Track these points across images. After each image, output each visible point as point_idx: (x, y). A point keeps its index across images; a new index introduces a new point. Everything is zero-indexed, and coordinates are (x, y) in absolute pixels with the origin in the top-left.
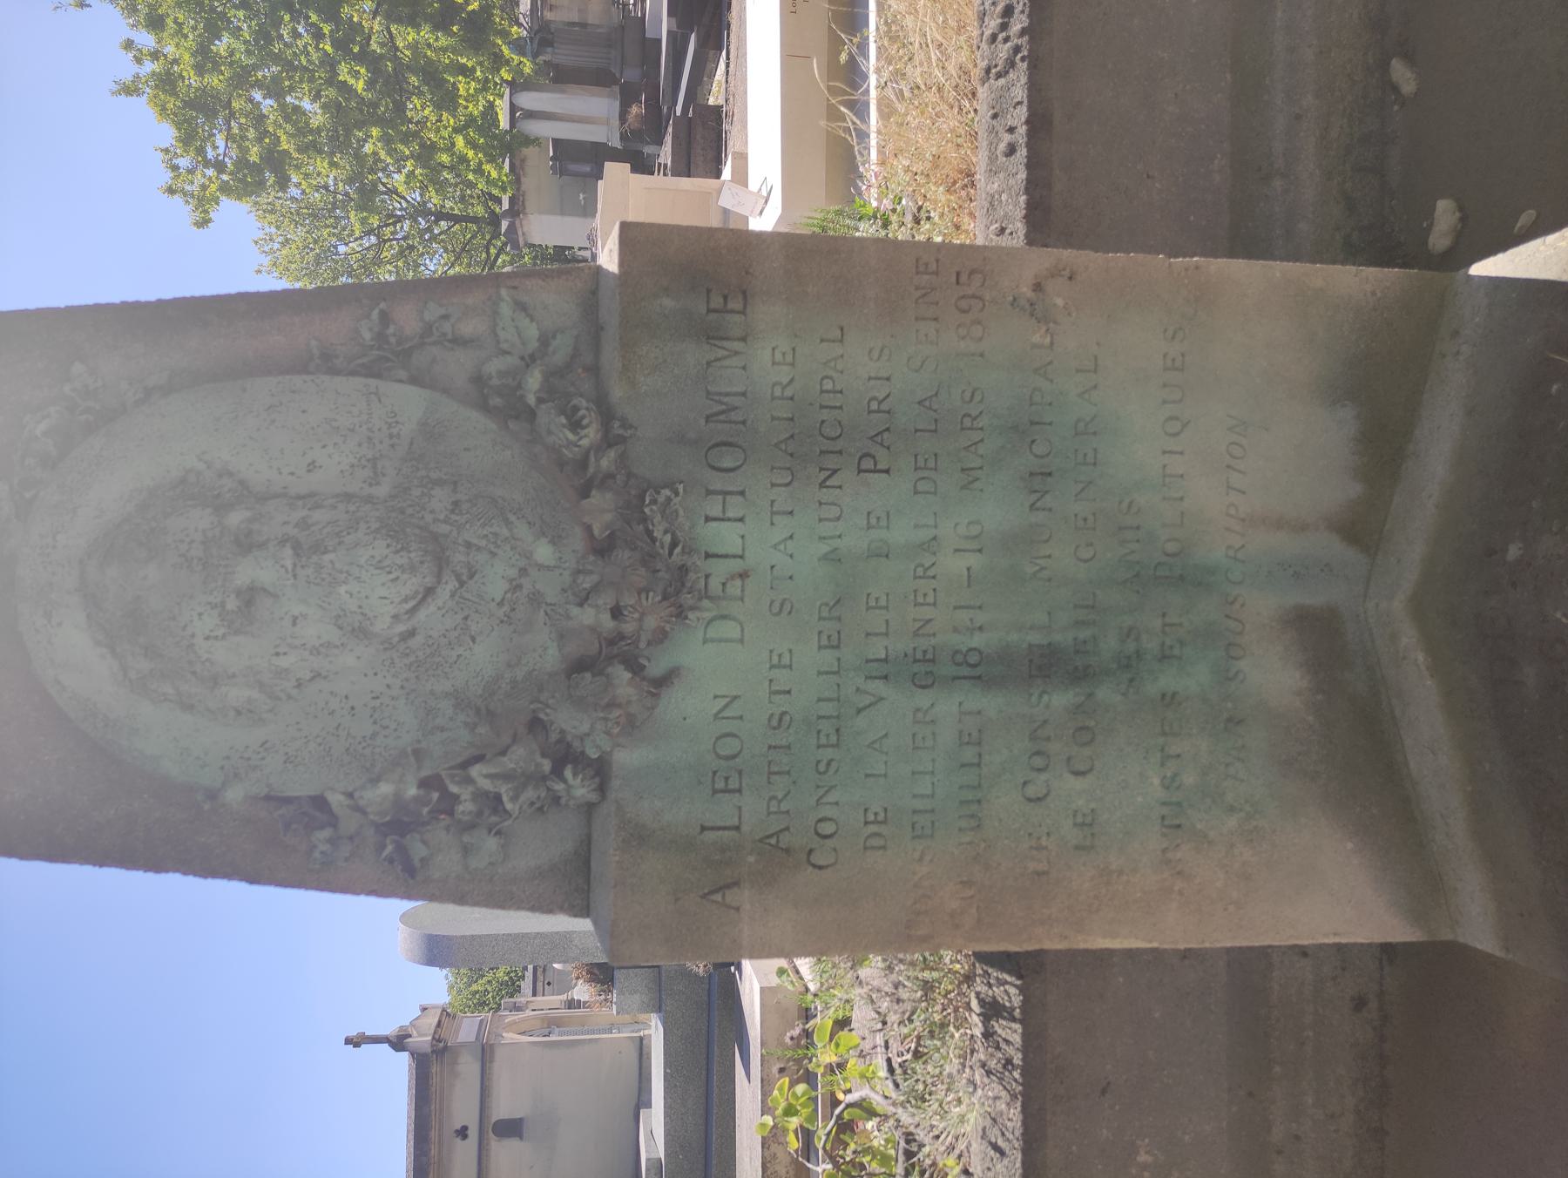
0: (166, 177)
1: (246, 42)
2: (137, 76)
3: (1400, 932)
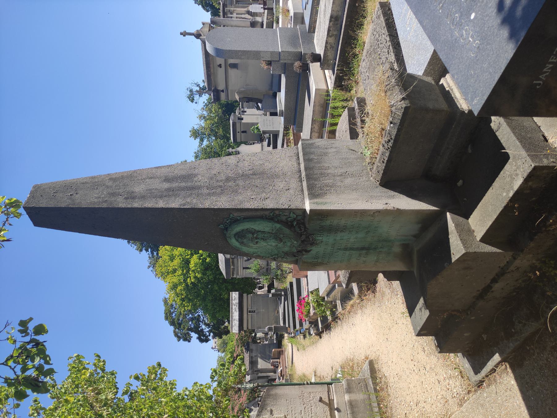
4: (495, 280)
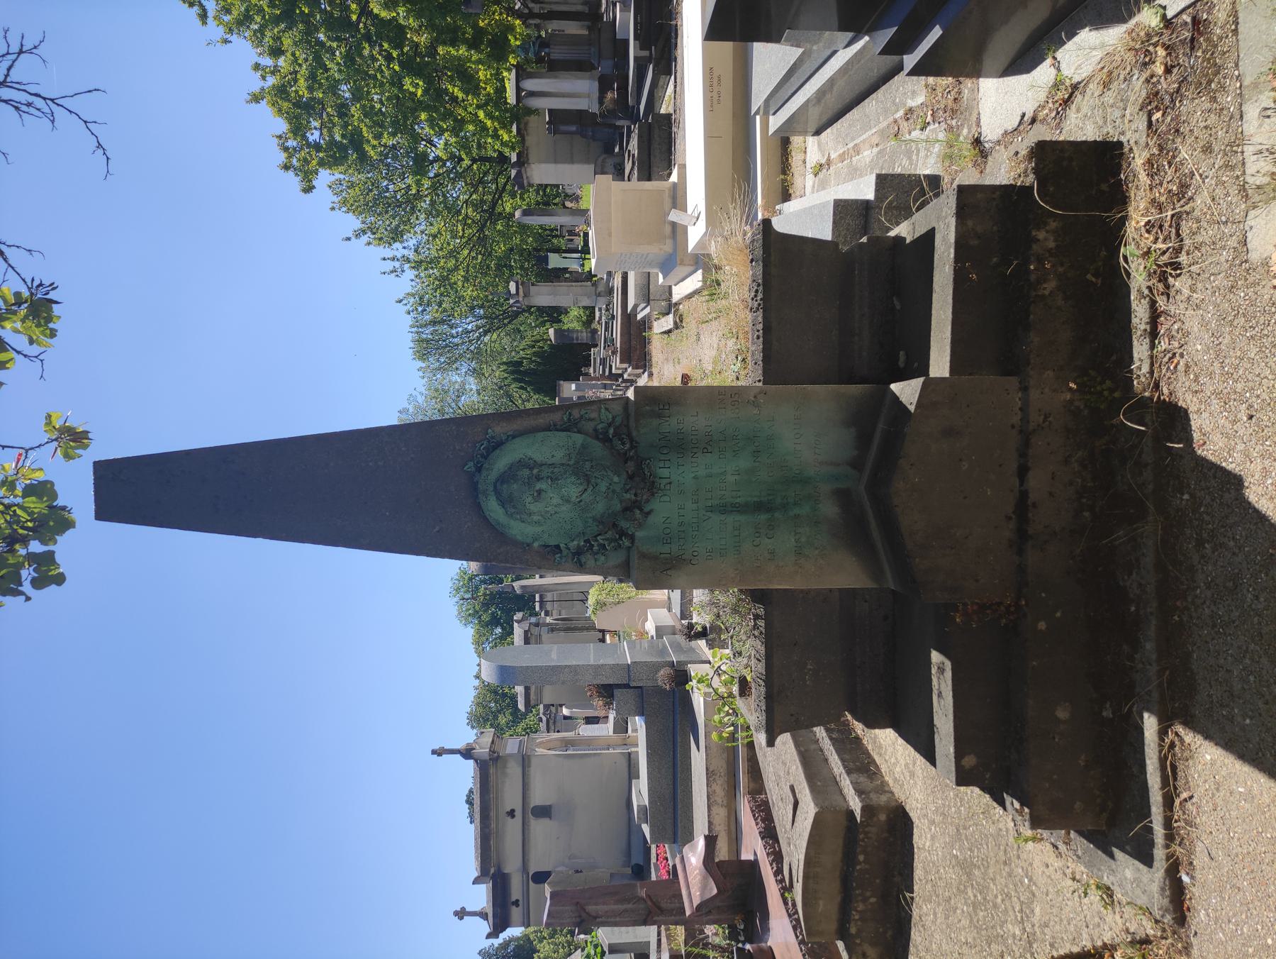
0: (282, 157)
1: (338, 64)
2: (263, 89)
3: (870, 584)
4: (1023, 472)
